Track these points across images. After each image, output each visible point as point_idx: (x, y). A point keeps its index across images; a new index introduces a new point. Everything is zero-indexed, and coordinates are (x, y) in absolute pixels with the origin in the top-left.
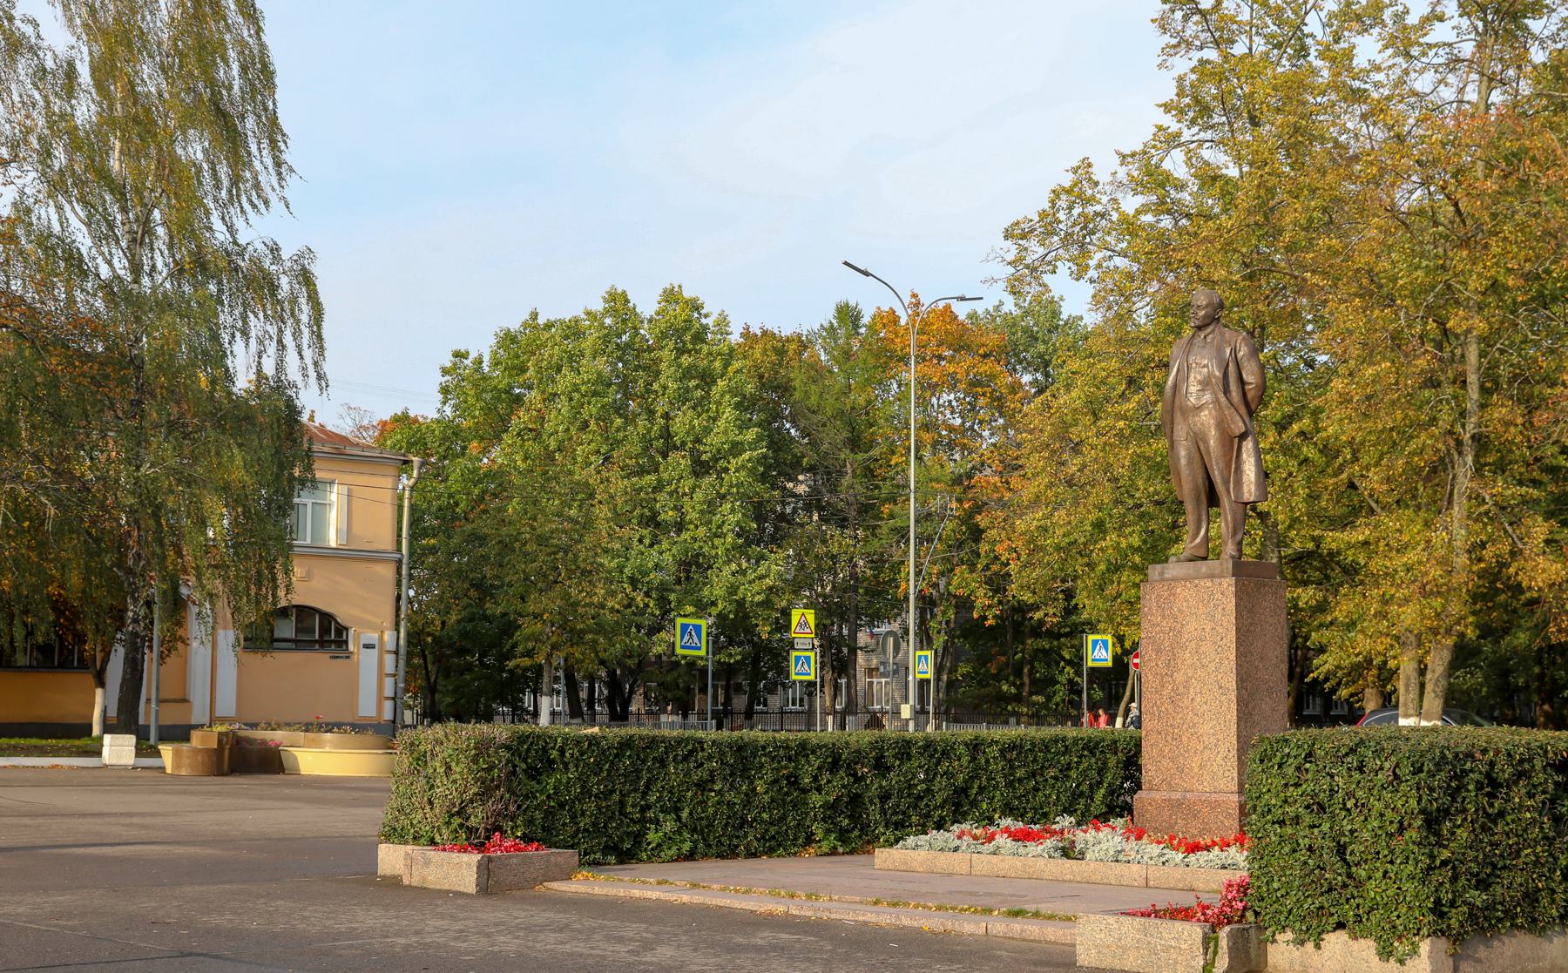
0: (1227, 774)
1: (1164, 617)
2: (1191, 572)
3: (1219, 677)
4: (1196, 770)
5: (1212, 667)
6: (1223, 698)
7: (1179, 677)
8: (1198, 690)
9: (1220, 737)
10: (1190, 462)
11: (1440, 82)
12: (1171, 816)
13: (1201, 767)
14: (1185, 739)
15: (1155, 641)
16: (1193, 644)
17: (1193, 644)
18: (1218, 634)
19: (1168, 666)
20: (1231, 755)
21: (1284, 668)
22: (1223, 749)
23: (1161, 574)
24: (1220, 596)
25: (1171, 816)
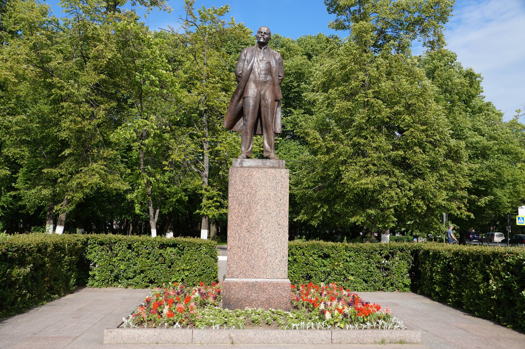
0: (281, 269)
1: (244, 186)
2: (260, 164)
3: (279, 219)
4: (262, 267)
5: (274, 214)
6: (280, 230)
7: (253, 218)
8: (265, 225)
9: (278, 250)
10: (255, 107)
11: (466, 102)
12: (248, 292)
13: (265, 265)
14: (255, 251)
15: (237, 199)
16: (263, 202)
17: (263, 202)
18: (278, 197)
19: (246, 212)
20: (284, 259)
21: (231, 190)
22: (279, 257)
23: (241, 163)
24: (280, 178)
25: (248, 292)
